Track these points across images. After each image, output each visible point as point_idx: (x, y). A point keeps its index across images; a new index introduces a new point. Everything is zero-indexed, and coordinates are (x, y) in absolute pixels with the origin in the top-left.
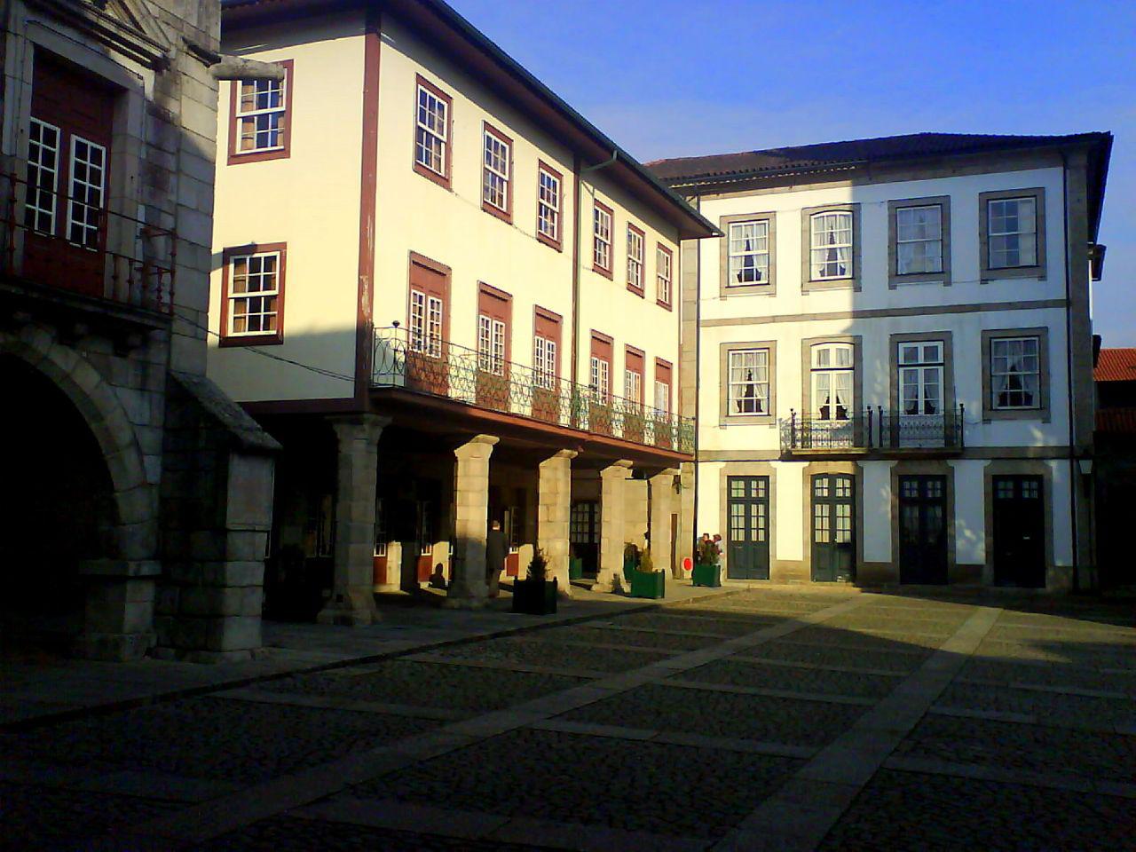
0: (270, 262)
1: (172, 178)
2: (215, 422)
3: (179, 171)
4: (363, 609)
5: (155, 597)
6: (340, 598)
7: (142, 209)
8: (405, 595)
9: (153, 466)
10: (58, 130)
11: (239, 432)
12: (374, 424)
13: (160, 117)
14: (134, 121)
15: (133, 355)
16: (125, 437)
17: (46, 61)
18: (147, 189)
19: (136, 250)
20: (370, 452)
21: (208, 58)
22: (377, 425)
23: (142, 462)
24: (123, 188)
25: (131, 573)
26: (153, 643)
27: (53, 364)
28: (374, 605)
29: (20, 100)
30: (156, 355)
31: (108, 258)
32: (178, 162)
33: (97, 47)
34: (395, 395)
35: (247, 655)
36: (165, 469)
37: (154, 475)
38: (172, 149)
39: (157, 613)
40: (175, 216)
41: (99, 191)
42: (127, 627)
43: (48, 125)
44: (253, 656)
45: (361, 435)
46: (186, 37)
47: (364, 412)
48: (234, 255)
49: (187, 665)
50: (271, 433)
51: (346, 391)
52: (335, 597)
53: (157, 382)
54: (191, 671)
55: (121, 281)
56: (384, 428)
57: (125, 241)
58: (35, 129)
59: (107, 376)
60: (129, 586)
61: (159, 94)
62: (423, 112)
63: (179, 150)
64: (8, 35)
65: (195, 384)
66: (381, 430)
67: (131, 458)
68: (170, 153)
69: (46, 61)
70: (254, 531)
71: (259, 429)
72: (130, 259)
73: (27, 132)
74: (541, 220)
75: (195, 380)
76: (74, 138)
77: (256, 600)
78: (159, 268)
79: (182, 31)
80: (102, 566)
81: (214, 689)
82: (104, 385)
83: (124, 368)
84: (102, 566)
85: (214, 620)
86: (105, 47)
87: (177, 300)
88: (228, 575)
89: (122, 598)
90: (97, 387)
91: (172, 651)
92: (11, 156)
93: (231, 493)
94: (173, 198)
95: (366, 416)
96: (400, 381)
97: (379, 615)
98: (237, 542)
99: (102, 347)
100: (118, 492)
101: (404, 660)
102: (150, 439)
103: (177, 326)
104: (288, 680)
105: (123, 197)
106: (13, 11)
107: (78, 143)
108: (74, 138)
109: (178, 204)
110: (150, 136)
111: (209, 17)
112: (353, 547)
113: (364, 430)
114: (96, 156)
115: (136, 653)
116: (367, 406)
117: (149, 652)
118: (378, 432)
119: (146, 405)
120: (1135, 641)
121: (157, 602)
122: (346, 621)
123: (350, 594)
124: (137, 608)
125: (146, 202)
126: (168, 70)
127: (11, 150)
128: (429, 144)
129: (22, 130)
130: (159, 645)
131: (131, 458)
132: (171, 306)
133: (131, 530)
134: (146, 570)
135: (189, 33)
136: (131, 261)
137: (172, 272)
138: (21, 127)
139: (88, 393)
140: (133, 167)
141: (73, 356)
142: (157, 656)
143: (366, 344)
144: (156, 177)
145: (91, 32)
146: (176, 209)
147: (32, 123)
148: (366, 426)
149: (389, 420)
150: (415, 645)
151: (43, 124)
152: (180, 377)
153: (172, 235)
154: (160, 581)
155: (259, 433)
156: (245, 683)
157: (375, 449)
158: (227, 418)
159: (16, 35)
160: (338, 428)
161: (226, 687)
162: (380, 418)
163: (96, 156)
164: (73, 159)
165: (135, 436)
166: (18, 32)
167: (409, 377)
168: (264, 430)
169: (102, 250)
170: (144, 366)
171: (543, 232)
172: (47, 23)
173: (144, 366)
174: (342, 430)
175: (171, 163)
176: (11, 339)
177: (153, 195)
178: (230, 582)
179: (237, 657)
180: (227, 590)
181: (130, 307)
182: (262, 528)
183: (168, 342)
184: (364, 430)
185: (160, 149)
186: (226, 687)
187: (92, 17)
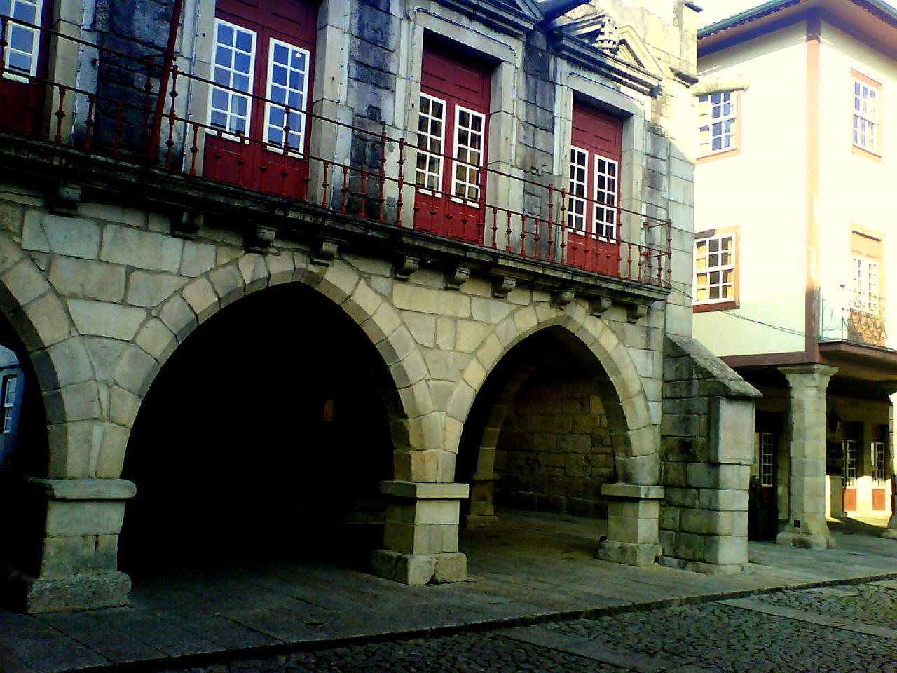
0: (726, 241)
1: (665, 180)
2: (706, 374)
3: (669, 173)
4: (819, 536)
5: (660, 516)
6: (797, 524)
7: (644, 206)
8: (838, 523)
9: (656, 409)
10: (254, 34)
11: (726, 382)
12: (823, 374)
13: (655, 131)
14: (637, 137)
15: (640, 321)
16: (635, 387)
17: (582, 103)
18: (647, 189)
19: (640, 238)
20: (819, 398)
21: (689, 81)
22: (825, 375)
23: (647, 406)
24: (631, 191)
25: (642, 497)
26: (660, 553)
27: (586, 331)
28: (829, 531)
29: (564, 133)
30: (656, 321)
31: (488, 211)
32: (669, 167)
33: (612, 85)
34: (843, 348)
35: (739, 570)
36: (664, 413)
37: (656, 418)
38: (665, 157)
39: (662, 529)
40: (667, 209)
41: (440, 142)
42: (640, 539)
43: (243, 30)
44: (743, 570)
45: (813, 383)
46: (673, 67)
47: (814, 364)
48: (701, 238)
49: (688, 573)
50: (750, 382)
51: (797, 344)
52: (792, 522)
53: (658, 342)
54: (695, 581)
55: (632, 266)
56: (831, 377)
57: (632, 231)
58: (424, 104)
59: (622, 339)
60: (641, 504)
61: (654, 115)
62: (857, 101)
63: (669, 157)
64: (556, 86)
65: (687, 343)
66: (829, 379)
67: (639, 402)
68: (662, 160)
69: (582, 103)
70: (740, 465)
71: (740, 380)
72: (639, 246)
73: (417, 106)
74: (855, 133)
75: (686, 341)
76: (458, 108)
77: (743, 522)
78: (659, 251)
79: (669, 63)
80: (619, 489)
81: (723, 597)
82: (621, 346)
83: (634, 332)
84: (619, 489)
85: (710, 536)
86: (619, 84)
87: (673, 277)
88: (721, 501)
89: (637, 516)
90: (616, 347)
91: (675, 561)
92: (560, 176)
93: (722, 433)
94: (665, 195)
95: (816, 366)
96: (845, 335)
97: (833, 541)
98: (726, 473)
99: (619, 316)
100: (630, 430)
101: (877, 586)
102: (654, 388)
103: (673, 297)
104: (780, 595)
105: (631, 199)
106: (559, 69)
107: (600, 160)
108: (458, 108)
109: (670, 200)
110: (649, 150)
111: (688, 49)
112: (807, 480)
113: (814, 379)
114: (438, 111)
115: (648, 560)
116: (817, 358)
117: (657, 559)
118: (825, 382)
119: (650, 361)
120: (2, 188)
121: (661, 520)
122: (804, 544)
123: (807, 521)
124: (647, 521)
125: (646, 200)
126: (661, 95)
127: (559, 172)
128: (862, 126)
129: (413, 105)
130: (664, 555)
131: (639, 402)
132: (668, 282)
133: (641, 461)
134: (653, 494)
135: (675, 64)
136: (640, 247)
137: (669, 254)
138: (412, 102)
139: (610, 353)
140: (638, 175)
141: (599, 323)
142: (663, 564)
143: (814, 305)
144: (653, 180)
145: (609, 74)
146: (668, 204)
147: (422, 98)
148: (816, 375)
149: (835, 370)
150: (883, 572)
151: (432, 98)
152: (674, 339)
153: (668, 223)
154: (665, 503)
155: (742, 382)
156: (742, 595)
157: (824, 395)
158: (714, 370)
159: (561, 85)
160: (789, 377)
161: (732, 596)
162: (828, 368)
163: (438, 111)
164: (457, 126)
165: (642, 386)
166: (563, 84)
167: (853, 332)
168: (745, 380)
169: (483, 204)
170: (648, 330)
171: (858, 145)
172: (581, 73)
173: (648, 330)
174: (793, 380)
175: (663, 167)
176: (560, 313)
177: (651, 194)
178: (722, 507)
179: (731, 570)
180: (720, 513)
181: (640, 285)
182: (746, 463)
183: (664, 310)
184: (814, 379)
185: (656, 158)
186: (732, 596)
187: (610, 62)
